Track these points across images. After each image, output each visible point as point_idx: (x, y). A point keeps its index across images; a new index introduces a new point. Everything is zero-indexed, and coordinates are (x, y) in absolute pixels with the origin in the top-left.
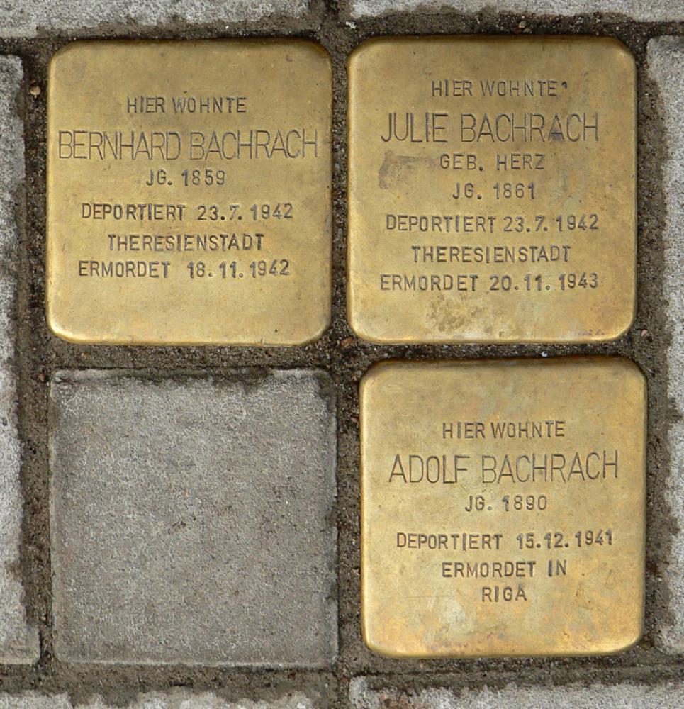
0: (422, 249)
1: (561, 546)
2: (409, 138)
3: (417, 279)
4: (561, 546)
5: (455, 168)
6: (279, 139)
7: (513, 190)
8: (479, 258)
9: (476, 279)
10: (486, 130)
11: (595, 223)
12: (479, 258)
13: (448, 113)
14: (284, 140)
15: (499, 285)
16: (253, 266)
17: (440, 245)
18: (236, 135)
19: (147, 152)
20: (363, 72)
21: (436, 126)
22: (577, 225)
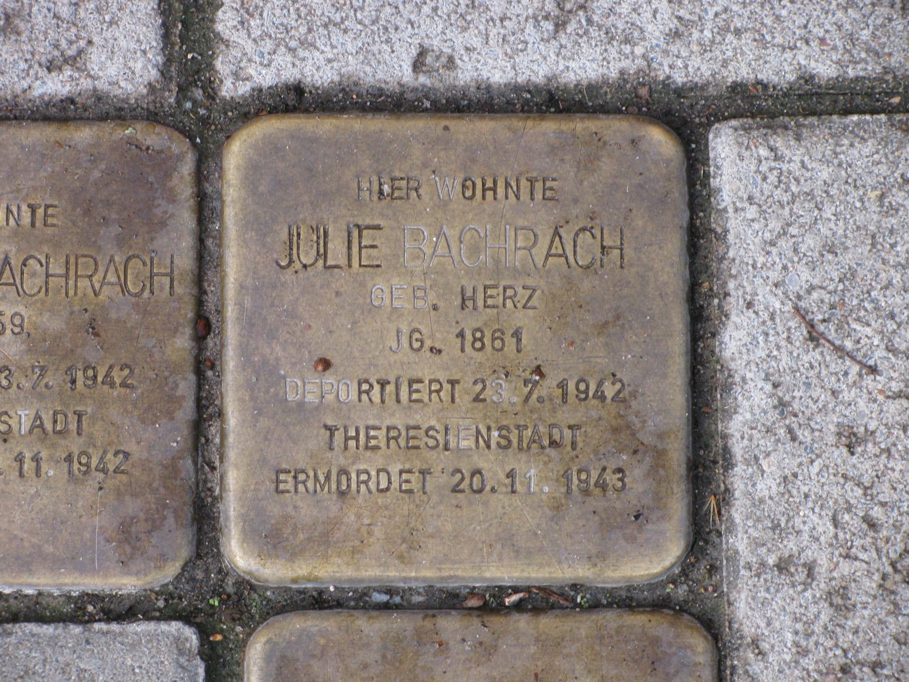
0: (342, 429)
1: (462, 491)
2: (321, 263)
3: (334, 477)
4: (462, 491)
5: (408, 448)
6: (112, 268)
7: (487, 341)
8: (431, 443)
9: (428, 477)
10: (557, 249)
11: (619, 392)
12: (431, 443)
13: (382, 223)
14: (121, 269)
15: (465, 485)
16: (69, 459)
17: (371, 423)
18: (44, 261)
19: (14, 284)
20: (252, 171)
21: (363, 244)
22: (591, 394)
